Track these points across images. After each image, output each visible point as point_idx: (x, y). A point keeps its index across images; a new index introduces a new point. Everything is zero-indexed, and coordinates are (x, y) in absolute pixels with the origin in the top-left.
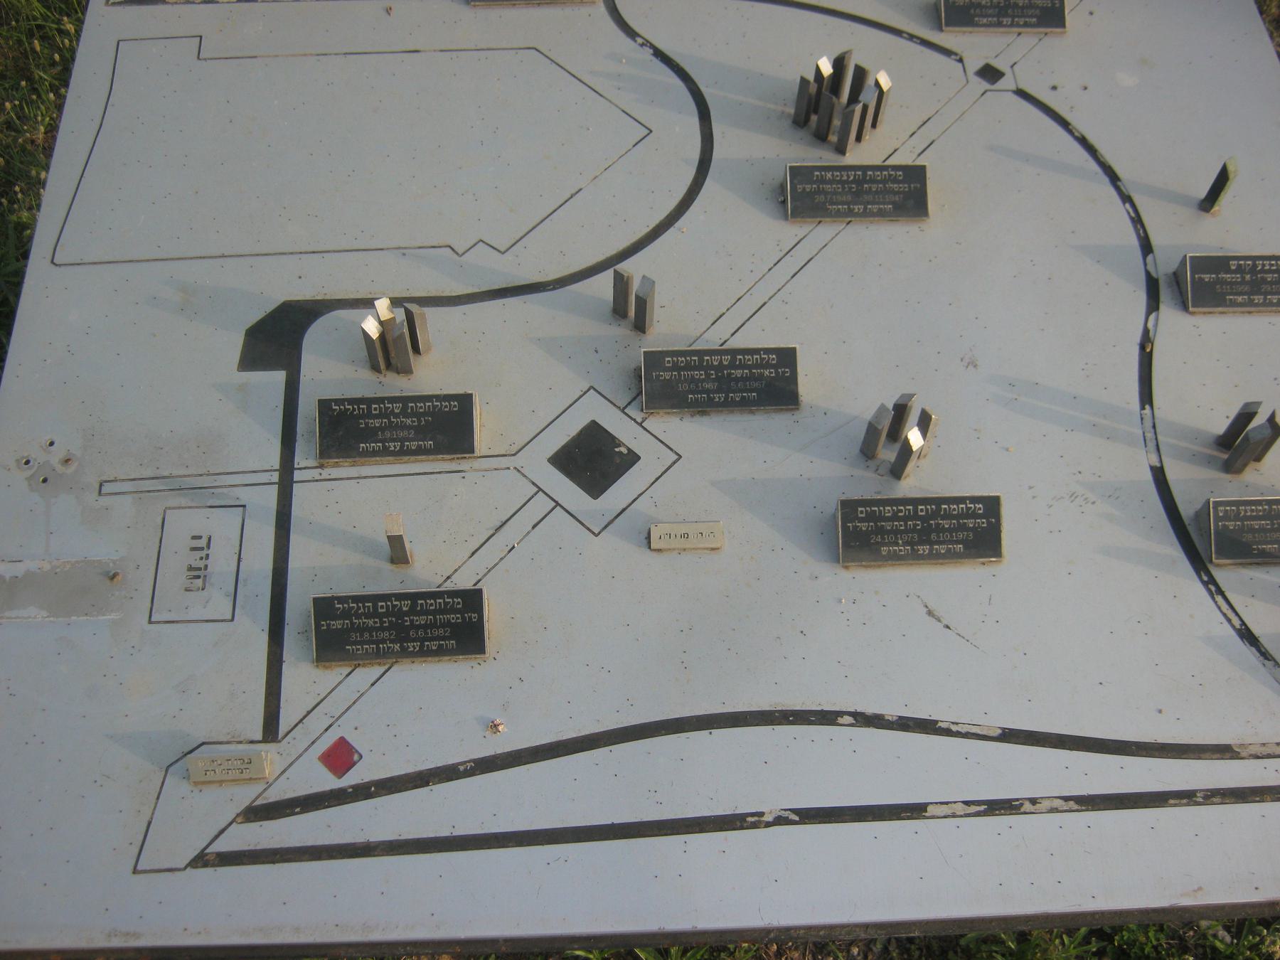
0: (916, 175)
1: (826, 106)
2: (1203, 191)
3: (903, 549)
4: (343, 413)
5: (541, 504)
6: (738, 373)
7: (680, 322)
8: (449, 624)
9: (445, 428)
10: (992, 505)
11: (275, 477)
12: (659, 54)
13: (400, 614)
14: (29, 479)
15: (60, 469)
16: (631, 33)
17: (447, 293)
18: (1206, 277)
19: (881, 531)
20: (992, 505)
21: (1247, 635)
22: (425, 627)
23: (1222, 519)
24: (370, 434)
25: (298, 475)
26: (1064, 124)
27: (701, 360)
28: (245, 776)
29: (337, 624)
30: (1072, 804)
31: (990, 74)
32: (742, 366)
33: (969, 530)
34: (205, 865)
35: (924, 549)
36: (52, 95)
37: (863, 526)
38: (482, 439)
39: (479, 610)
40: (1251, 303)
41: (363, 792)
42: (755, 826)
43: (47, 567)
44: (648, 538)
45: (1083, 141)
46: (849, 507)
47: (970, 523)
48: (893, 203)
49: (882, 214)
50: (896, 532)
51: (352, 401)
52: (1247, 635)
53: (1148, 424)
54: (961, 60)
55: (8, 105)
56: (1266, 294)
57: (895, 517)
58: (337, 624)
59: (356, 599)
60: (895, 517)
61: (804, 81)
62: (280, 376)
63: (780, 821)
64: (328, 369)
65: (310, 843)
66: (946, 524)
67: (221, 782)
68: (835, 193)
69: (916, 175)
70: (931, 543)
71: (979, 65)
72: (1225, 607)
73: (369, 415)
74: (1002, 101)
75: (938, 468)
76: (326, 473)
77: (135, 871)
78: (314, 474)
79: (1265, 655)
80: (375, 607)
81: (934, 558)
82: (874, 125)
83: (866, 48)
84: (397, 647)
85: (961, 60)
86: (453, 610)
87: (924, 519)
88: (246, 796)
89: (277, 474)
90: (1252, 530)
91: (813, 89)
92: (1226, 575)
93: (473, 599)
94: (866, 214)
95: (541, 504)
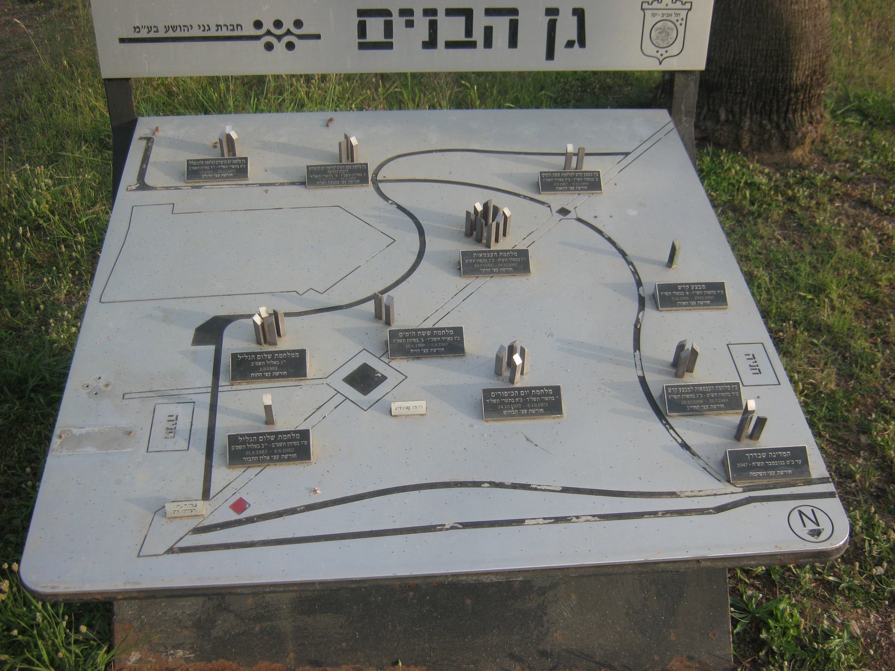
0: (524, 254)
1: (479, 225)
2: (666, 258)
3: (514, 412)
4: (243, 359)
5: (339, 398)
6: (435, 339)
7: (407, 317)
8: (293, 446)
9: (294, 366)
10: (557, 390)
11: (210, 390)
12: (400, 207)
13: (270, 442)
14: (88, 393)
15: (104, 388)
16: (386, 198)
17: (295, 311)
18: (667, 294)
19: (503, 403)
20: (557, 390)
21: (685, 446)
22: (282, 448)
23: (670, 394)
24: (256, 369)
25: (220, 389)
26: (600, 232)
27: (417, 333)
28: (193, 514)
29: (239, 447)
30: (596, 518)
31: (564, 212)
32: (437, 336)
33: (548, 402)
34: (173, 553)
35: (524, 411)
36: (70, 275)
37: (494, 401)
38: (311, 370)
39: (308, 439)
40: (690, 305)
41: (250, 520)
42: (440, 530)
43: (97, 430)
44: (391, 411)
45: (609, 240)
46: (487, 392)
47: (546, 399)
48: (513, 267)
49: (507, 272)
50: (510, 403)
51: (247, 354)
52: (685, 446)
53: (638, 357)
54: (549, 206)
55: (45, 279)
56: (697, 301)
57: (509, 397)
58: (239, 447)
59: (248, 435)
60: (509, 397)
61: (468, 213)
62: (212, 348)
63: (452, 528)
64: (235, 342)
65: (224, 542)
66: (534, 399)
67: (181, 517)
68: (484, 263)
69: (524, 254)
70: (528, 409)
71: (559, 208)
72: (674, 434)
73: (256, 360)
74: (570, 223)
75: (530, 377)
76: (234, 388)
77: (139, 556)
78: (229, 388)
79: (694, 454)
80: (258, 438)
81: (529, 415)
82: (504, 235)
83: (496, 199)
84: (268, 458)
85: (549, 206)
86: (296, 440)
87: (524, 397)
88: (194, 523)
89: (210, 394)
90: (685, 399)
91: (473, 217)
92: (675, 420)
93: (305, 434)
94: (499, 272)
95: (339, 398)
